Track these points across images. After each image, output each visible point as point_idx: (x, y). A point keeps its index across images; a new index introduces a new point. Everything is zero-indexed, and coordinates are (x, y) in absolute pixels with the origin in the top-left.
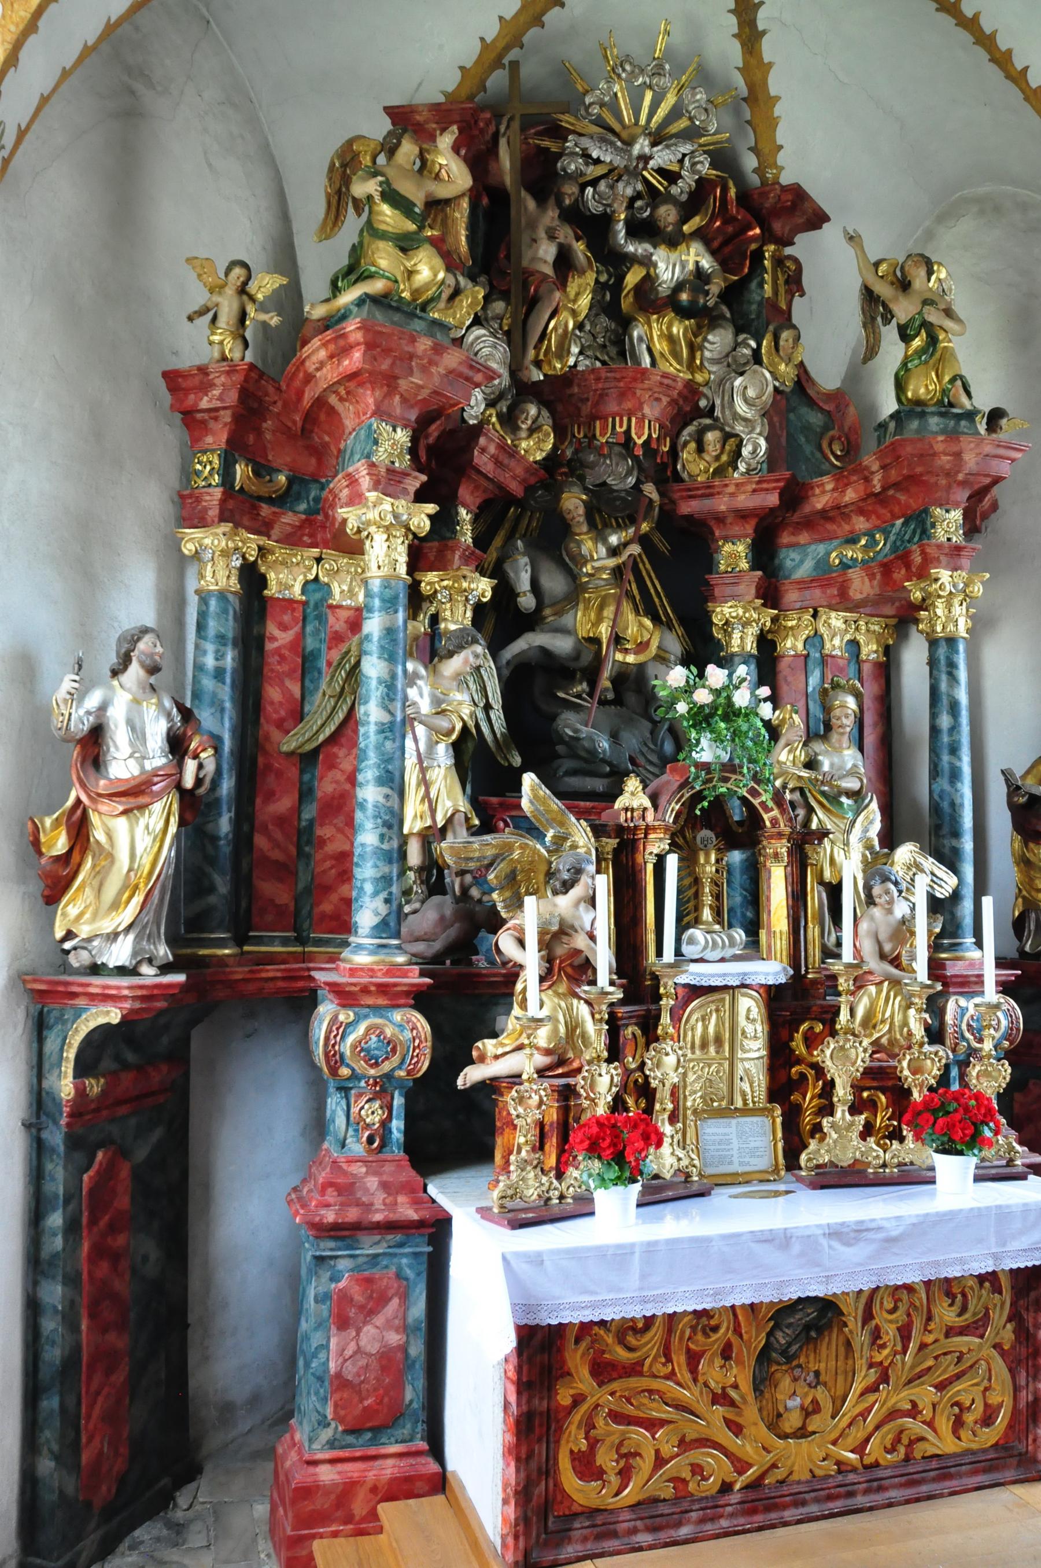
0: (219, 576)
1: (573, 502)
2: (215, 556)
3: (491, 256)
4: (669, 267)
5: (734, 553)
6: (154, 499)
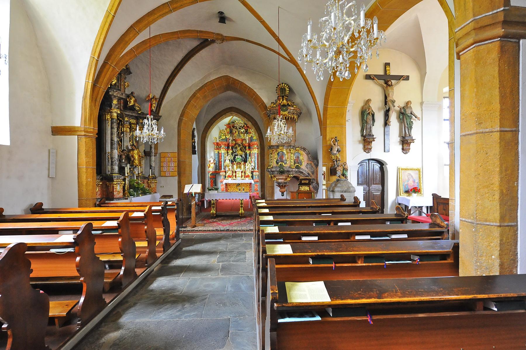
0: (216, 152)
1: (237, 146)
2: (216, 152)
3: (231, 132)
4: (242, 131)
5: (247, 148)
6: (213, 149)
